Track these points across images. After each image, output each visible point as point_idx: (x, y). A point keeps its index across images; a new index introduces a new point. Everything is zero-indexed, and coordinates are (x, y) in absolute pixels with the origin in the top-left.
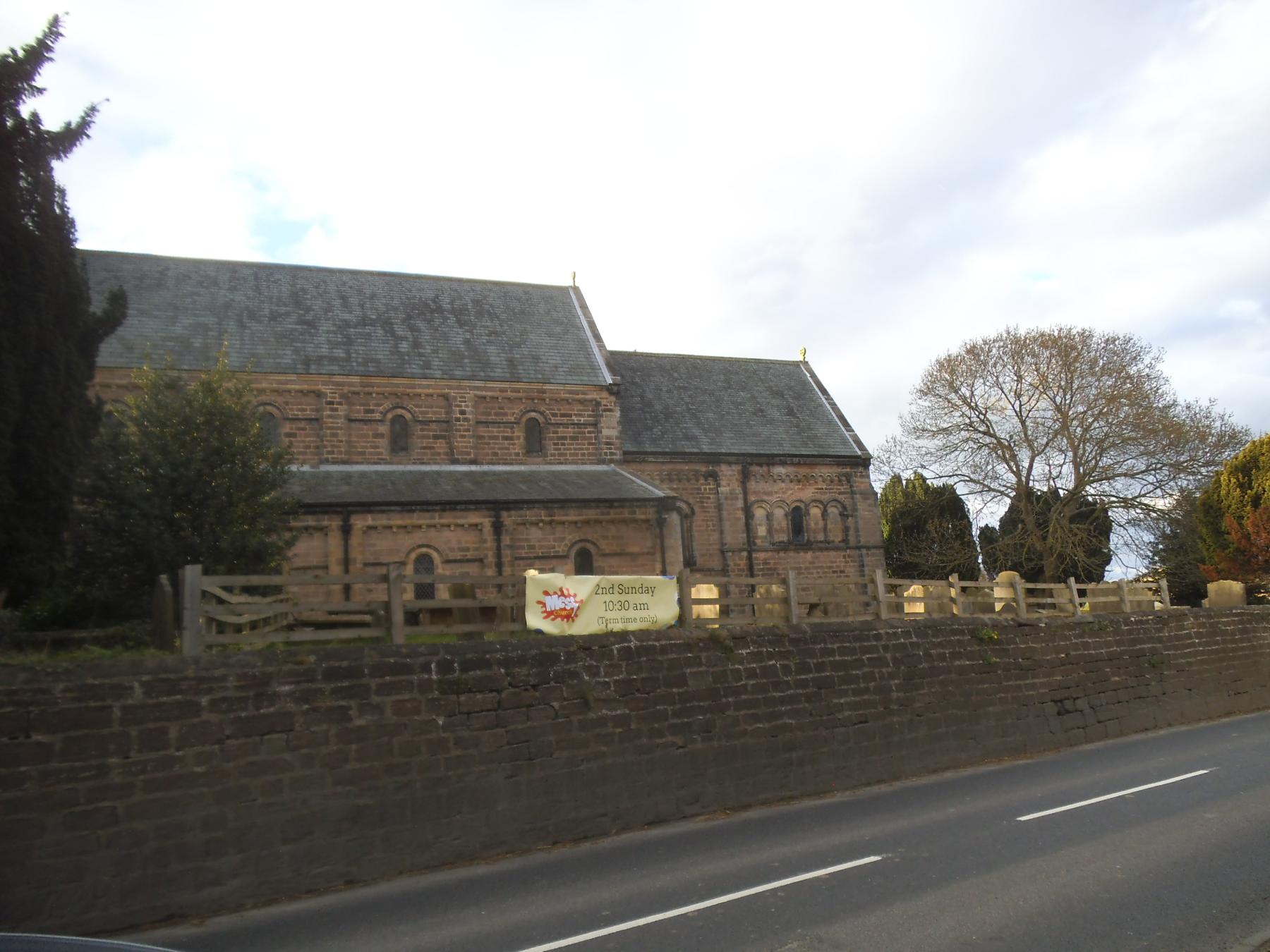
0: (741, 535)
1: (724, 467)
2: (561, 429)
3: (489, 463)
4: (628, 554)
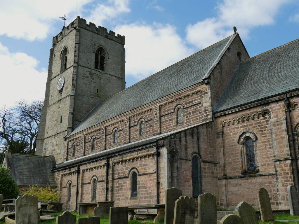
0: (285, 149)
1: (273, 105)
2: (189, 109)
3: (164, 133)
4: (147, 174)
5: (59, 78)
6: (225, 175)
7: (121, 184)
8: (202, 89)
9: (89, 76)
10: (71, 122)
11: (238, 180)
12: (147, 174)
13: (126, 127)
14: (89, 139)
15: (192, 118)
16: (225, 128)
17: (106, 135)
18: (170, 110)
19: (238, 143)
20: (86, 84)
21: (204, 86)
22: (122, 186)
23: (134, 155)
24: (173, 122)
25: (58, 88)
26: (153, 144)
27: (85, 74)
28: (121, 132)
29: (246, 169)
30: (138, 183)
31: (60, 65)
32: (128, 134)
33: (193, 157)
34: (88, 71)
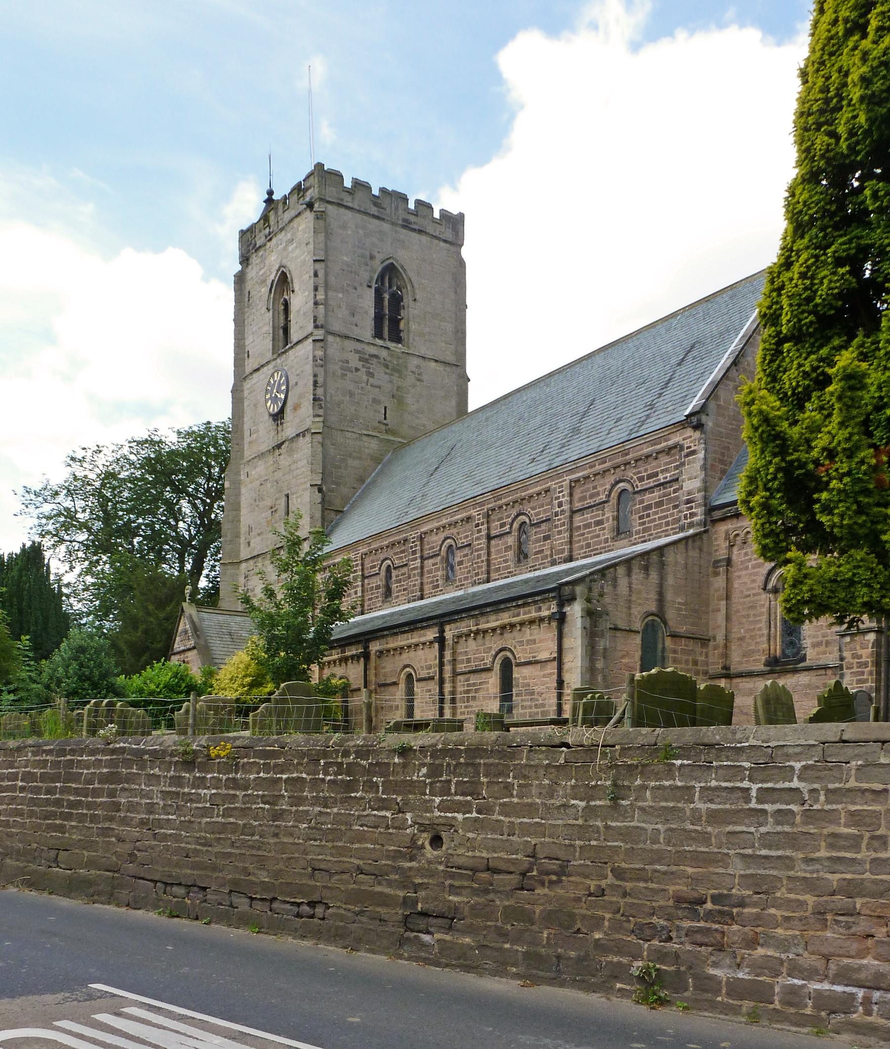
4: (537, 662)
5: (270, 372)
6: (726, 668)
7: (474, 684)
8: (684, 439)
9: (359, 365)
10: (318, 515)
11: (757, 679)
12: (537, 662)
13: (478, 539)
14: (374, 567)
15: (654, 520)
16: (735, 549)
17: (423, 559)
18: (598, 494)
19: (765, 589)
20: (351, 394)
21: (689, 432)
22: (477, 691)
23: (505, 618)
24: (604, 529)
25: (268, 405)
26: (551, 595)
27: (347, 362)
28: (466, 551)
29: (778, 652)
30: (514, 683)
31: (268, 328)
32: (484, 558)
33: (647, 625)
34: (357, 352)
